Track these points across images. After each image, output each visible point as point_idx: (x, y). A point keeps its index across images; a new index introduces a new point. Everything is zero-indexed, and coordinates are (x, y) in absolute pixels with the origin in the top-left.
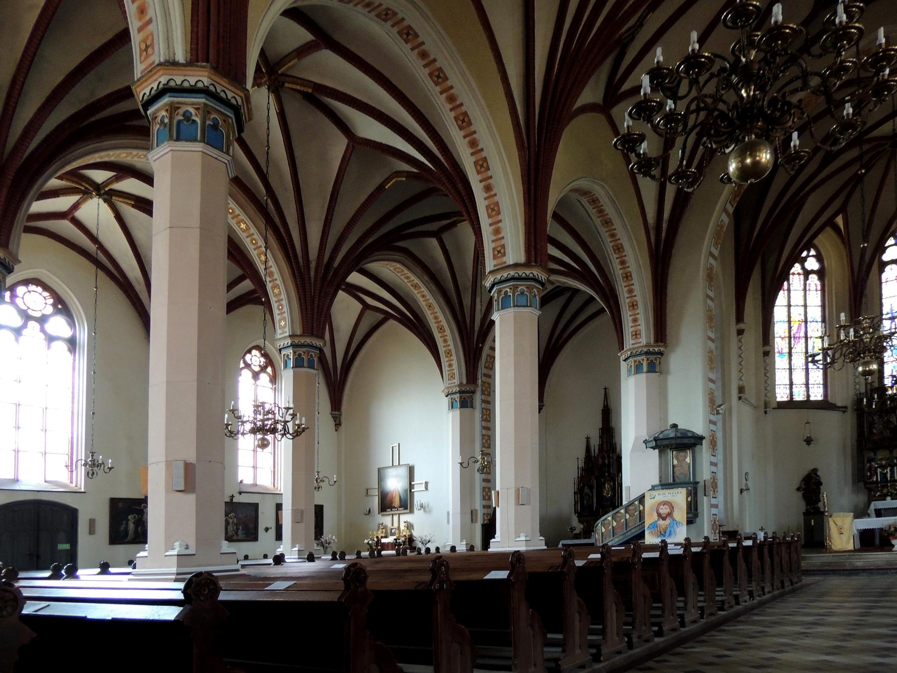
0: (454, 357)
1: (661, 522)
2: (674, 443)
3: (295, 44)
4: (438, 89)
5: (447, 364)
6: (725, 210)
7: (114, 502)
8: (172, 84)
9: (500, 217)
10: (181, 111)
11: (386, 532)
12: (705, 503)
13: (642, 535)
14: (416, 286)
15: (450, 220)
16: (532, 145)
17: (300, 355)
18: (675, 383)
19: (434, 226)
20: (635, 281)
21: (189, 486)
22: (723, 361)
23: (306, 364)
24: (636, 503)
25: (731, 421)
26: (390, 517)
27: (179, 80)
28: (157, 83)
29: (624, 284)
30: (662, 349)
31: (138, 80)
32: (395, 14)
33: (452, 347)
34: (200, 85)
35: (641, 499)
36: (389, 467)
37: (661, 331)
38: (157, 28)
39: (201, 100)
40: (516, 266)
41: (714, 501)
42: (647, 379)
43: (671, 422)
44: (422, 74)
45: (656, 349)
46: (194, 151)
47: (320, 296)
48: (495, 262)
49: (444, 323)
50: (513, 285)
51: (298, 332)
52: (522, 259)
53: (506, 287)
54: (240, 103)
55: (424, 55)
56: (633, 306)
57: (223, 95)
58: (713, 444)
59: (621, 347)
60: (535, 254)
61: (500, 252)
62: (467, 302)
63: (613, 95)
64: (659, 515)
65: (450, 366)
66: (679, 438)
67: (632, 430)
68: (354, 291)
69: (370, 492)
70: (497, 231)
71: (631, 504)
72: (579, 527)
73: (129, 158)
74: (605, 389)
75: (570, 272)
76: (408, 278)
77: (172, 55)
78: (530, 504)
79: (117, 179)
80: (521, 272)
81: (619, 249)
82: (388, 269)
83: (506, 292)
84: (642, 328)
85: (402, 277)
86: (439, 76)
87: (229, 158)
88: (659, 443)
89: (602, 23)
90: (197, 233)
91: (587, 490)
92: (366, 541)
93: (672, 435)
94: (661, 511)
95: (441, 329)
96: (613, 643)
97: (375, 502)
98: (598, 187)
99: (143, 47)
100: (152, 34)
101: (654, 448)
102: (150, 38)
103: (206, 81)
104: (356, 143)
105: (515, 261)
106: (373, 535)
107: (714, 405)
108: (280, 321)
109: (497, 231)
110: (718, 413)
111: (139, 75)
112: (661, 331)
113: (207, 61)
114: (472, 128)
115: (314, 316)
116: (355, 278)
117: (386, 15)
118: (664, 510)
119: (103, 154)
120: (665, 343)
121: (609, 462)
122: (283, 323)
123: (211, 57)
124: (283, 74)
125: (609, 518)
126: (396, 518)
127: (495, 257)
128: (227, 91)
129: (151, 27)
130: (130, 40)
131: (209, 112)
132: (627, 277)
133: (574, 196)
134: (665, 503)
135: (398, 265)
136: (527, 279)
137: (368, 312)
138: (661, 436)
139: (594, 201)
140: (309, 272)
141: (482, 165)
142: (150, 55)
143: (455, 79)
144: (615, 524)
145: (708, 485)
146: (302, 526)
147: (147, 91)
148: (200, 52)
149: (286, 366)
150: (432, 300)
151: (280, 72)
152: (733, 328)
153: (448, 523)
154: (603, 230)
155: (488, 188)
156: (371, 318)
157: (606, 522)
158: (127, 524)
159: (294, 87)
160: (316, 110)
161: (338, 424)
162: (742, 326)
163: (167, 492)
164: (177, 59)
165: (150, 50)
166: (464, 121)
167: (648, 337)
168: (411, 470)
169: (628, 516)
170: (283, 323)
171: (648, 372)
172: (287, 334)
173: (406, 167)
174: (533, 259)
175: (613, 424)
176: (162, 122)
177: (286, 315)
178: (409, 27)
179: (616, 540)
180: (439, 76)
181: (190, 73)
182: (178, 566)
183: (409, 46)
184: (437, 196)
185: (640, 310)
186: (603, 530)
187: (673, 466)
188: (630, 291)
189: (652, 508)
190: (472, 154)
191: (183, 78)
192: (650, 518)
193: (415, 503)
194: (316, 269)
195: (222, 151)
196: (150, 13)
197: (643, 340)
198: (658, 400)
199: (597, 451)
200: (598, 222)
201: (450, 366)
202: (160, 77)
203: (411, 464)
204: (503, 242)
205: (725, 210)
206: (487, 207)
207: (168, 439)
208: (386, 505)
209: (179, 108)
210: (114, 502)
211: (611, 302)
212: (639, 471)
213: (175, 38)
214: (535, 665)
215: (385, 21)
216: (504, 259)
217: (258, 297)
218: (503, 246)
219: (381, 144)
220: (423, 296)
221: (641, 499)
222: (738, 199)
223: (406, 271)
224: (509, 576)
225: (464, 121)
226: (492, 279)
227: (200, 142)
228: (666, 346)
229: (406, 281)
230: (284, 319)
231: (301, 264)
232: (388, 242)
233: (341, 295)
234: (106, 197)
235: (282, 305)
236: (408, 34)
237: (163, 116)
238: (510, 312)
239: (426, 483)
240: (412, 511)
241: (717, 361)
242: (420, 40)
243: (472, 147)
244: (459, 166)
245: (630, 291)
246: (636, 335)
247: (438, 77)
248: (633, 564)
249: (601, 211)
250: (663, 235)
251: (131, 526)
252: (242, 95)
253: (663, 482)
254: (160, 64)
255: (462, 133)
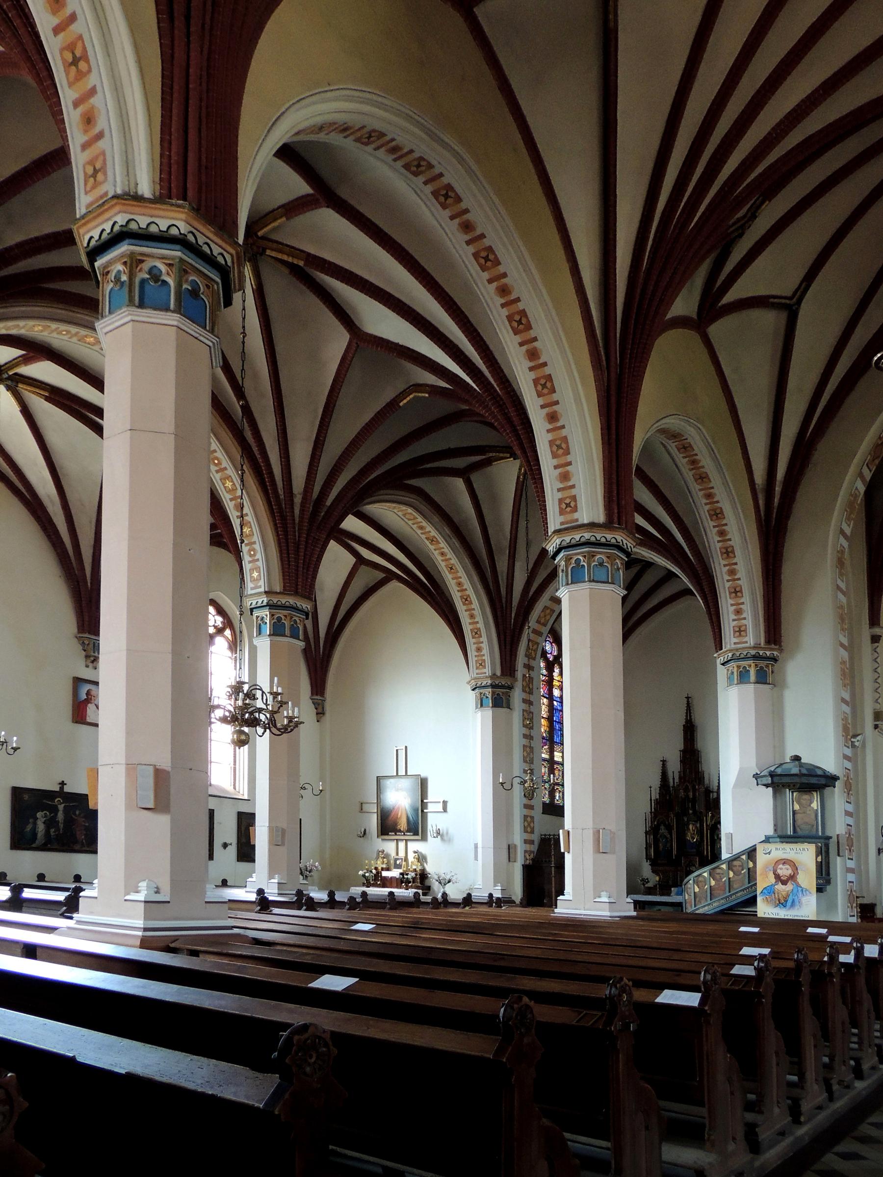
0: (484, 639)
1: (780, 887)
2: (796, 781)
3: (282, 198)
4: (486, 275)
5: (474, 647)
6: (861, 475)
7: (17, 793)
8: (133, 226)
9: (569, 458)
10: (146, 266)
11: (388, 863)
12: (838, 865)
13: (752, 901)
14: (432, 540)
15: (484, 456)
16: (612, 364)
17: (279, 619)
18: (792, 698)
19: (460, 463)
20: (739, 558)
21: (161, 803)
22: (853, 677)
23: (287, 632)
24: (744, 857)
25: (864, 759)
26: (393, 844)
27: (143, 221)
28: (111, 223)
29: (723, 562)
30: (775, 653)
31: (83, 217)
32: (430, 166)
33: (481, 625)
34: (174, 231)
35: (751, 853)
36: (392, 777)
37: (774, 630)
38: (111, 145)
39: (176, 253)
40: (592, 526)
41: (851, 864)
42: (755, 689)
43: (790, 752)
44: (462, 253)
45: (768, 653)
46: (167, 323)
47: (307, 542)
48: (562, 519)
49: (470, 592)
50: (588, 552)
51: (278, 588)
52: (601, 518)
53: (578, 554)
54: (229, 263)
55: (467, 227)
56: (736, 592)
57: (206, 249)
58: (848, 787)
59: (719, 646)
60: (619, 513)
61: (569, 505)
62: (502, 565)
63: (711, 309)
64: (778, 877)
65: (479, 649)
66: (804, 775)
67: (733, 759)
68: (347, 539)
69: (365, 807)
70: (565, 477)
71: (737, 857)
72: (654, 879)
73: (45, 333)
74: (688, 698)
75: (647, 540)
76: (421, 528)
77: (132, 186)
78: (614, 853)
79: (25, 360)
80: (600, 536)
81: (717, 514)
82: (395, 514)
83: (578, 561)
84: (749, 623)
85: (414, 527)
86: (487, 258)
87: (215, 340)
88: (776, 779)
89: (707, 209)
90: (171, 441)
91: (663, 830)
92: (361, 873)
93: (795, 771)
94: (779, 871)
95: (466, 600)
96: (813, 1095)
97: (373, 822)
98: (692, 429)
99: (90, 170)
100: (103, 153)
101: (767, 786)
102: (101, 158)
103: (184, 228)
104: (362, 341)
105: (591, 520)
106: (371, 865)
107: (850, 733)
108: (252, 570)
109: (565, 477)
110: (853, 746)
111: (84, 211)
112: (774, 630)
113: (185, 199)
114: (532, 333)
115: (297, 571)
116: (351, 524)
117: (419, 166)
118: (785, 871)
119: (10, 324)
120: (780, 646)
121: (694, 795)
122: (255, 574)
123: (190, 193)
124: (263, 238)
125: (705, 874)
126: (402, 845)
127: (562, 512)
128: (212, 245)
129: (101, 144)
130: (70, 163)
131: (186, 272)
132: (727, 553)
133: (662, 438)
134: (785, 862)
135: (410, 510)
136: (607, 545)
137: (363, 568)
138: (779, 771)
139: (686, 448)
140: (293, 508)
141: (545, 385)
142: (101, 183)
143: (511, 263)
144: (713, 883)
145: (843, 841)
146: (283, 850)
147: (96, 234)
148: (174, 184)
149: (260, 633)
150: (454, 561)
151: (260, 234)
152: (866, 632)
153: (476, 858)
154: (695, 487)
155: (552, 417)
156: (366, 577)
157: (700, 879)
158: (35, 824)
159: (280, 256)
160: (308, 292)
161: (320, 713)
162: (877, 631)
163: (128, 807)
164: (140, 193)
165: (100, 176)
166: (520, 323)
167: (756, 636)
168: (423, 783)
169: (731, 874)
170: (255, 574)
171: (757, 682)
172: (262, 590)
173: (431, 379)
174: (616, 519)
175: (700, 745)
176: (117, 279)
177: (260, 564)
178: (449, 187)
179: (715, 904)
180: (487, 258)
181: (161, 213)
182: (146, 919)
183: (447, 213)
184: (483, 420)
185: (746, 598)
186: (697, 890)
187: (794, 812)
188: (732, 572)
189: (766, 867)
190: (531, 369)
191: (150, 220)
192: (764, 881)
193: (429, 827)
194: (303, 504)
195: (205, 328)
196: (101, 124)
197: (750, 639)
198: (771, 722)
199: (677, 780)
200: (689, 475)
201: (479, 649)
202: (116, 214)
203: (423, 775)
204: (573, 492)
205: (861, 475)
206: (551, 443)
207: (129, 733)
208: (388, 826)
209: (143, 261)
210: (17, 793)
211: (705, 584)
212: (744, 817)
213: (137, 163)
214: (734, 1139)
215: (416, 174)
216: (576, 515)
217: (223, 536)
218: (574, 498)
219: (397, 345)
220: (442, 554)
221: (751, 853)
222: (877, 462)
223: (420, 519)
224: (703, 1001)
225: (520, 323)
226: (558, 541)
227: (173, 312)
228: (781, 650)
229: (419, 532)
230: (258, 569)
231: (282, 497)
232: (398, 477)
233: (333, 546)
234: (9, 383)
235: (254, 550)
236: (446, 196)
237: (119, 272)
238: (584, 589)
239: (445, 803)
240: (424, 838)
241: (848, 675)
242: (463, 205)
243: (531, 360)
244: (510, 385)
245: (732, 572)
246: (740, 631)
247: (487, 259)
248: (831, 975)
249: (694, 462)
250: (776, 500)
251: (41, 827)
252: (234, 252)
253: (780, 833)
254: (115, 197)
255: (518, 339)
